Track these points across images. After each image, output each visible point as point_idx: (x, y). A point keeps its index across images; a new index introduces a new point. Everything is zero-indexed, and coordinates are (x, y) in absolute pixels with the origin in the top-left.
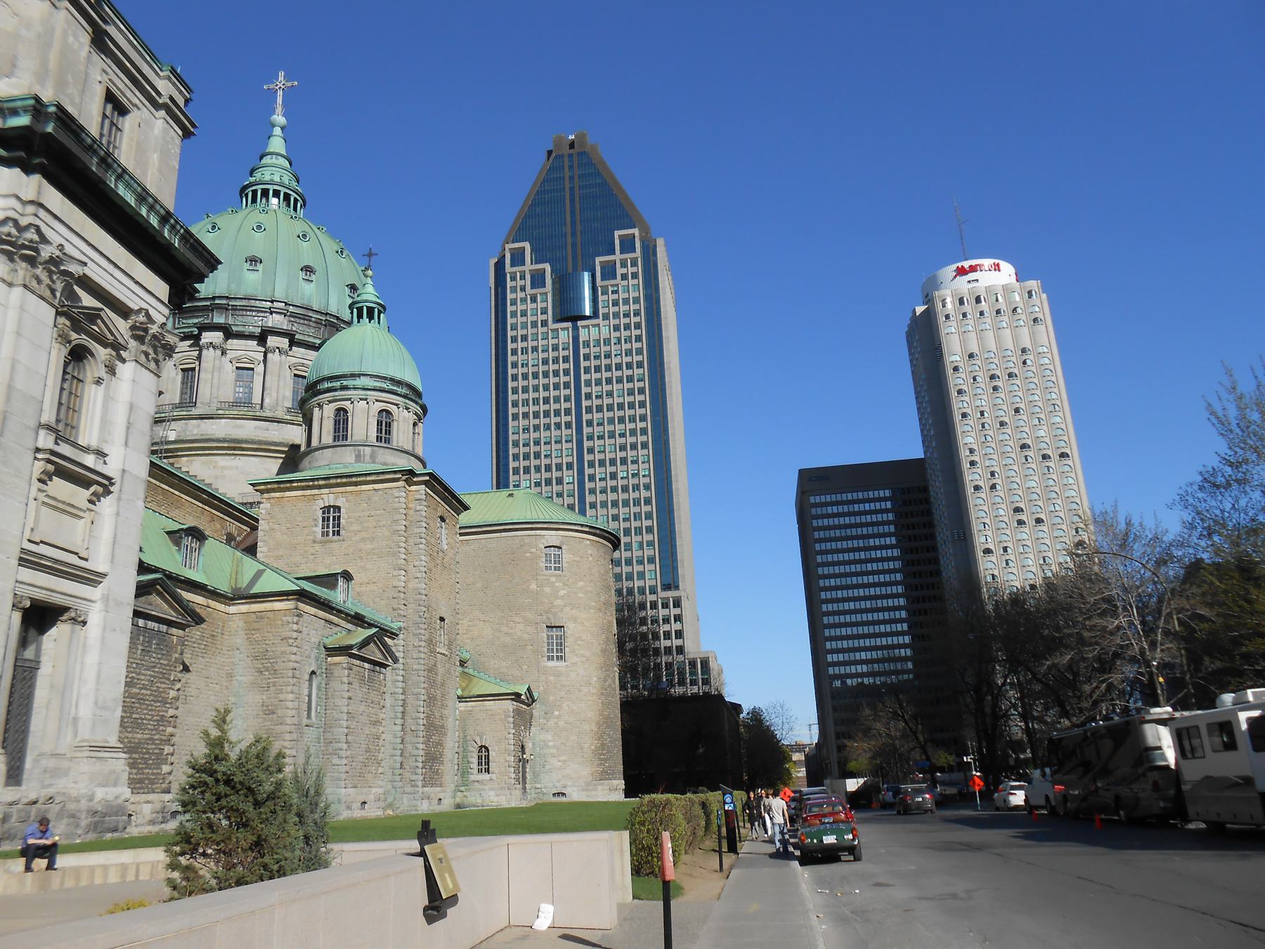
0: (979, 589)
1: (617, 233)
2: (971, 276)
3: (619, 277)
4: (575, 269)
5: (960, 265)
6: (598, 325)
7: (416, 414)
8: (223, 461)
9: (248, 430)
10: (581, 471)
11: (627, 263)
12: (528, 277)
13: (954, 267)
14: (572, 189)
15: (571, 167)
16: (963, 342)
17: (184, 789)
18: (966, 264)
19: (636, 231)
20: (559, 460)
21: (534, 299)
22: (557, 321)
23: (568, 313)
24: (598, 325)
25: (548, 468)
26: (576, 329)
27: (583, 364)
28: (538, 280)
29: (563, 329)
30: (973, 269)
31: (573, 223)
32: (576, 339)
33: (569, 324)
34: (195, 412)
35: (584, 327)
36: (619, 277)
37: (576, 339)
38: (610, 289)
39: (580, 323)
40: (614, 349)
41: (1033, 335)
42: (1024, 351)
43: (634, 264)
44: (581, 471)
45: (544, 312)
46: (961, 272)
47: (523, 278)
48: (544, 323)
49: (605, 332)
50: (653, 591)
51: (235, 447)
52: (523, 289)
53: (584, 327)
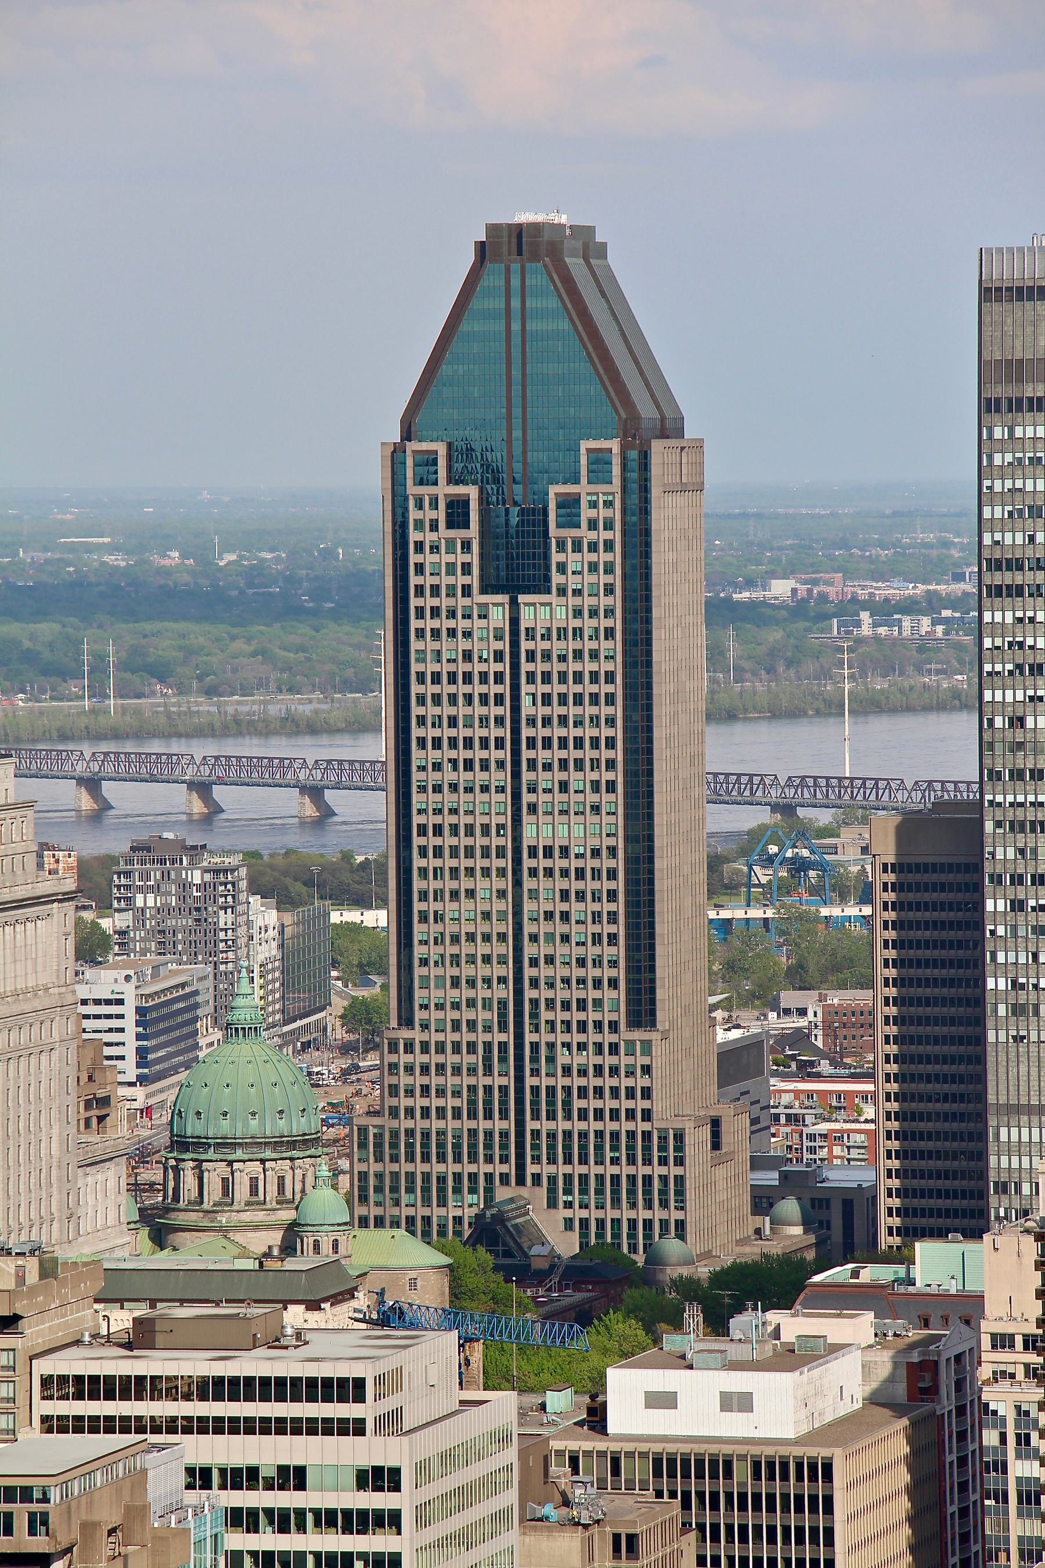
1: (585, 445)
3: (584, 524)
6: (550, 604)
8: (250, 1234)
9: (260, 1216)
10: (516, 796)
12: (442, 505)
20: (485, 820)
22: (483, 591)
24: (550, 604)
25: (470, 830)
26: (514, 603)
27: (525, 667)
29: (494, 605)
32: (515, 621)
34: (234, 1208)
35: (526, 604)
36: (584, 524)
37: (515, 621)
40: (576, 932)
44: (516, 796)
45: (467, 569)
47: (434, 504)
48: (467, 591)
49: (560, 613)
50: (614, 1026)
51: (256, 1227)
53: (526, 604)
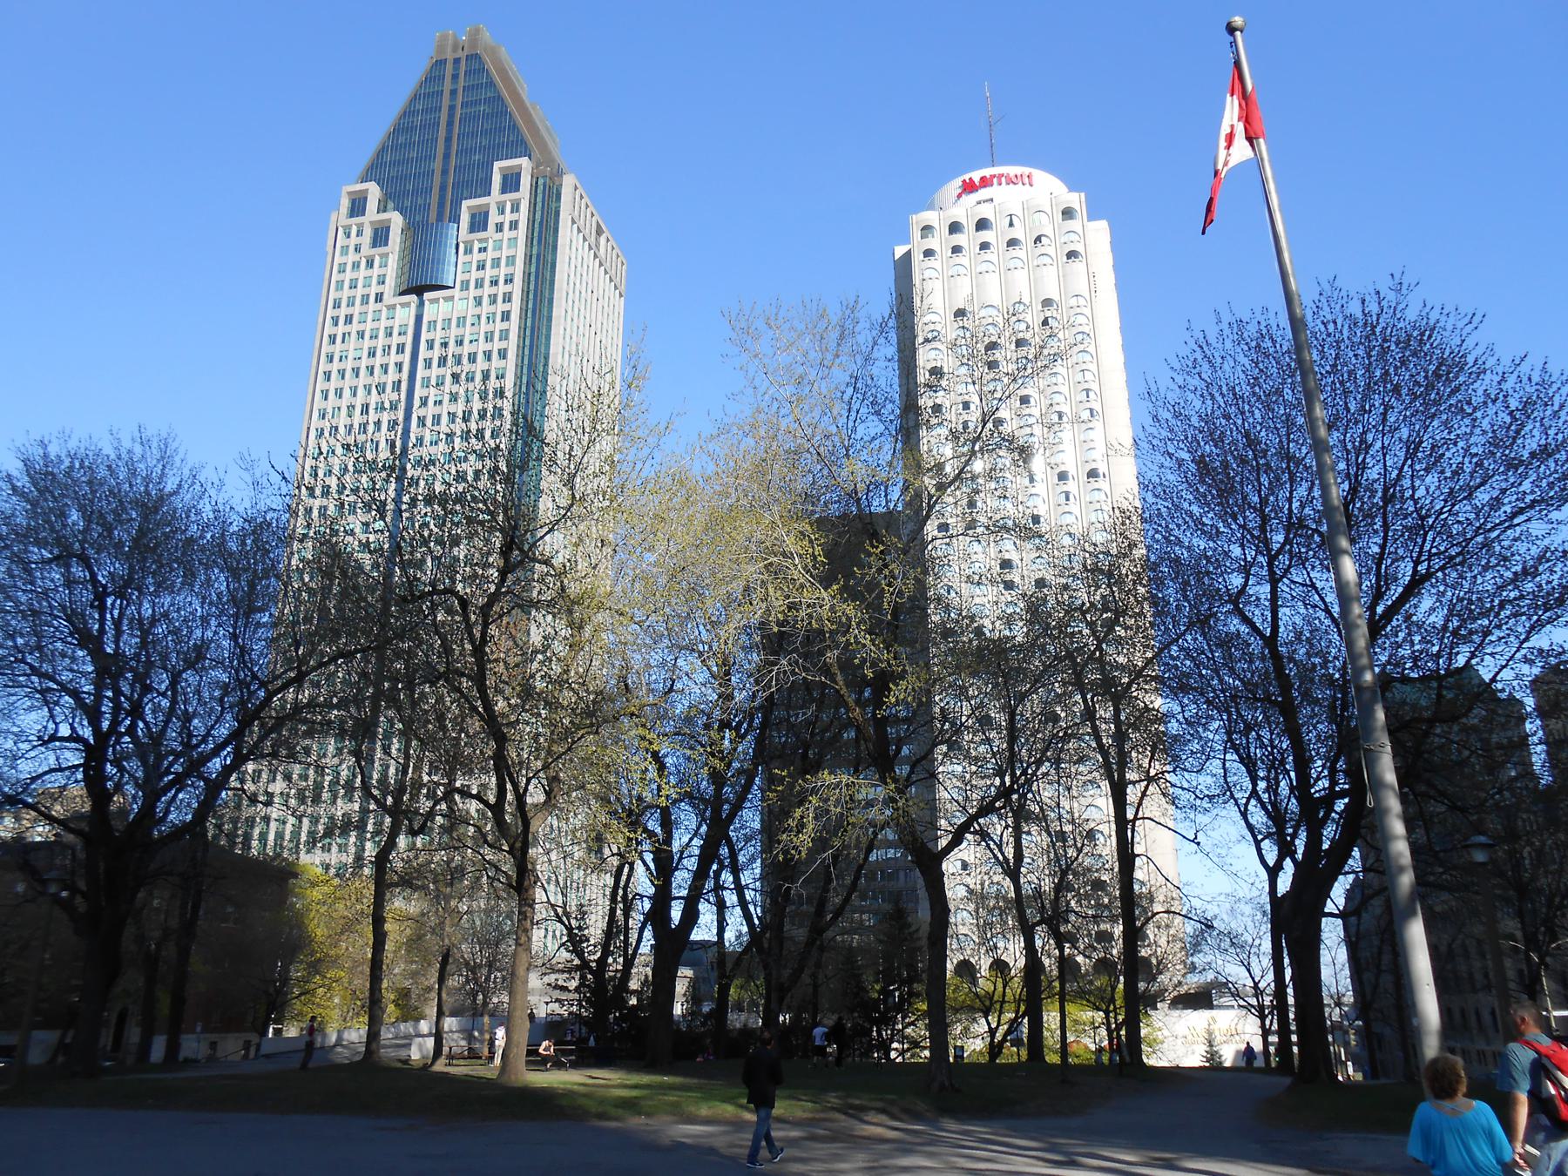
0: (712, 1151)
2: (983, 193)
4: (440, 218)
5: (967, 177)
7: (965, 425)
11: (509, 212)
13: (958, 182)
14: (452, 108)
15: (455, 77)
16: (948, 292)
17: (972, 618)
18: (976, 176)
19: (524, 162)
21: (370, 264)
23: (418, 286)
26: (421, 304)
28: (380, 236)
29: (403, 305)
30: (985, 182)
31: (447, 156)
32: (419, 319)
33: (414, 297)
37: (419, 319)
38: (476, 246)
39: (427, 295)
41: (1063, 280)
42: (1047, 303)
43: (516, 208)
46: (969, 187)
52: (357, 249)
